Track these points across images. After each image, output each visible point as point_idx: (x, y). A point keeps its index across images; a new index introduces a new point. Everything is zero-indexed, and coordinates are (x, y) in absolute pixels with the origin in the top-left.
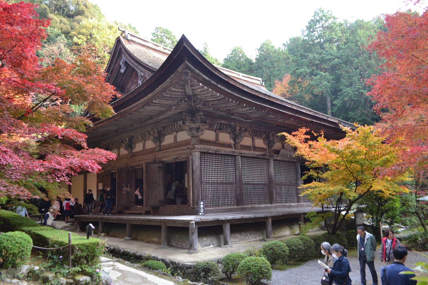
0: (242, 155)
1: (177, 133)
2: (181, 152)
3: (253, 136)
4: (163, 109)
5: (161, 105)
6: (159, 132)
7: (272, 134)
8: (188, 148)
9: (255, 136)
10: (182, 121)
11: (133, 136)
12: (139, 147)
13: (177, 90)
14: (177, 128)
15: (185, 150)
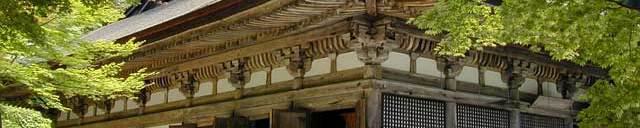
1: (337, 54)
2: (345, 92)
4: (318, 12)
8: (359, 84)
10: (349, 34)
11: (247, 58)
12: (257, 79)
14: (339, 46)
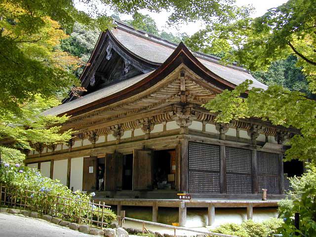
0: (227, 145)
3: (237, 127)
4: (157, 101)
5: (156, 98)
6: (149, 121)
7: (256, 126)
8: (177, 137)
9: (240, 127)
13: (172, 87)
14: (167, 118)
15: (174, 138)
